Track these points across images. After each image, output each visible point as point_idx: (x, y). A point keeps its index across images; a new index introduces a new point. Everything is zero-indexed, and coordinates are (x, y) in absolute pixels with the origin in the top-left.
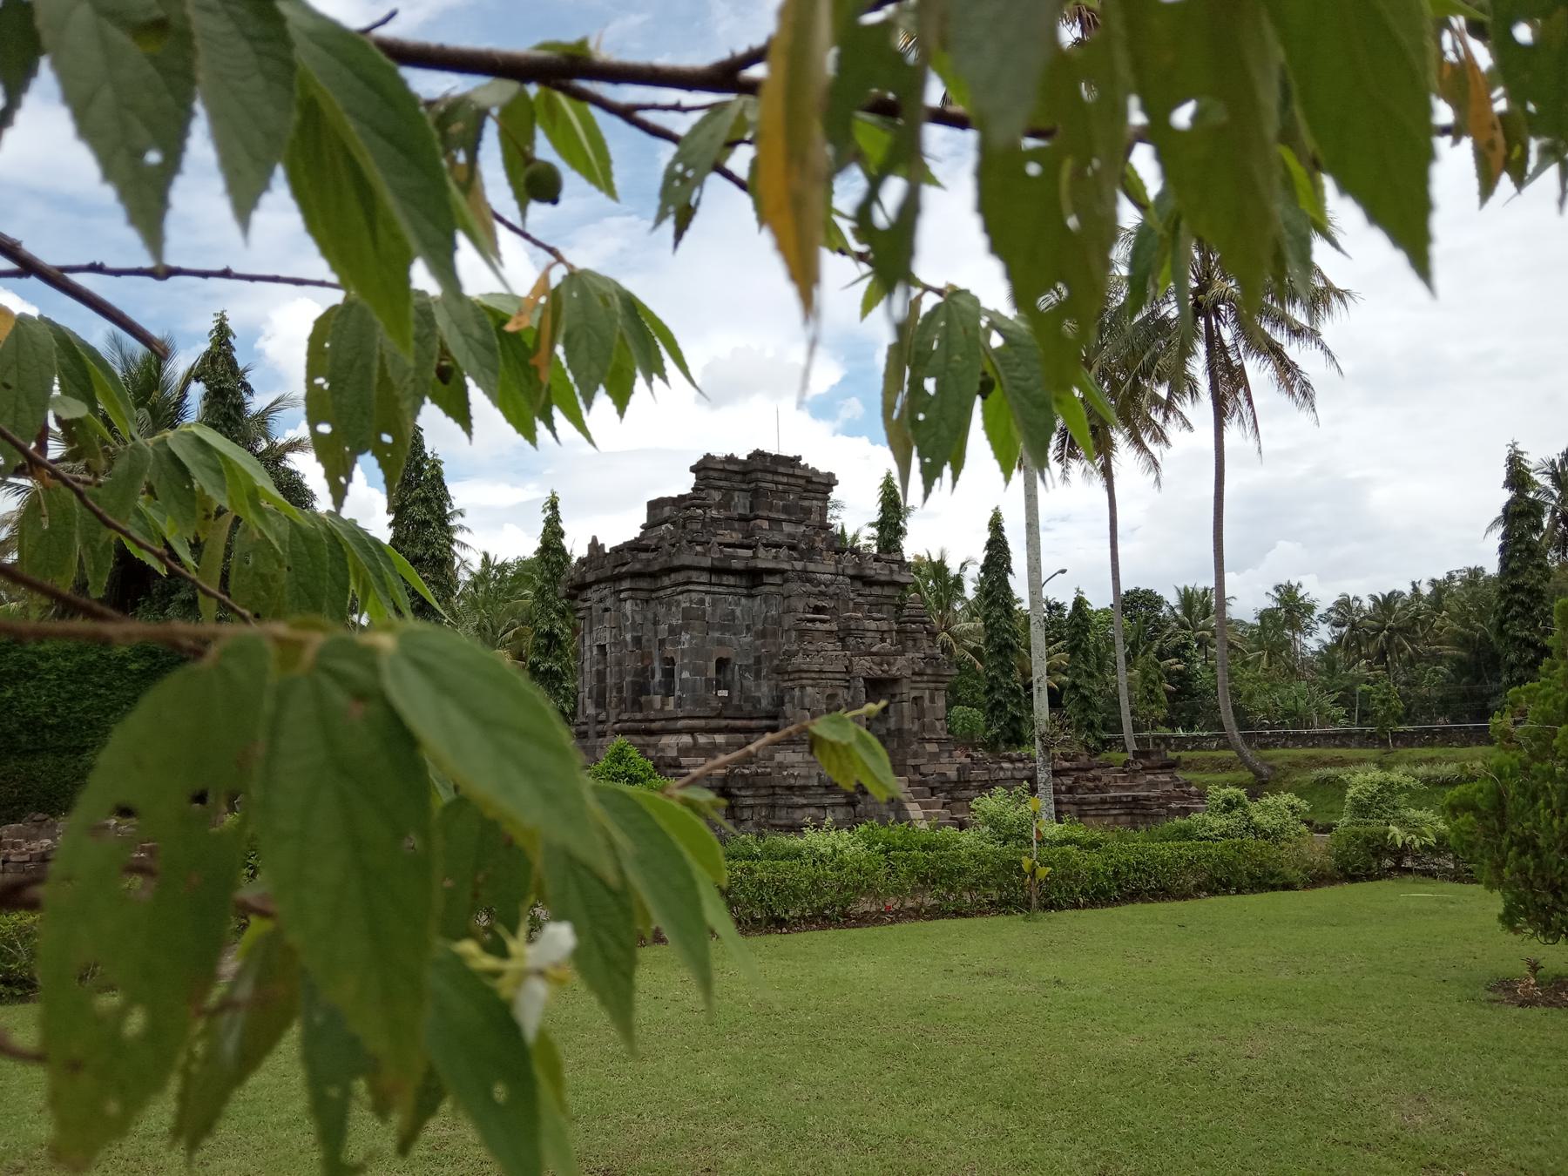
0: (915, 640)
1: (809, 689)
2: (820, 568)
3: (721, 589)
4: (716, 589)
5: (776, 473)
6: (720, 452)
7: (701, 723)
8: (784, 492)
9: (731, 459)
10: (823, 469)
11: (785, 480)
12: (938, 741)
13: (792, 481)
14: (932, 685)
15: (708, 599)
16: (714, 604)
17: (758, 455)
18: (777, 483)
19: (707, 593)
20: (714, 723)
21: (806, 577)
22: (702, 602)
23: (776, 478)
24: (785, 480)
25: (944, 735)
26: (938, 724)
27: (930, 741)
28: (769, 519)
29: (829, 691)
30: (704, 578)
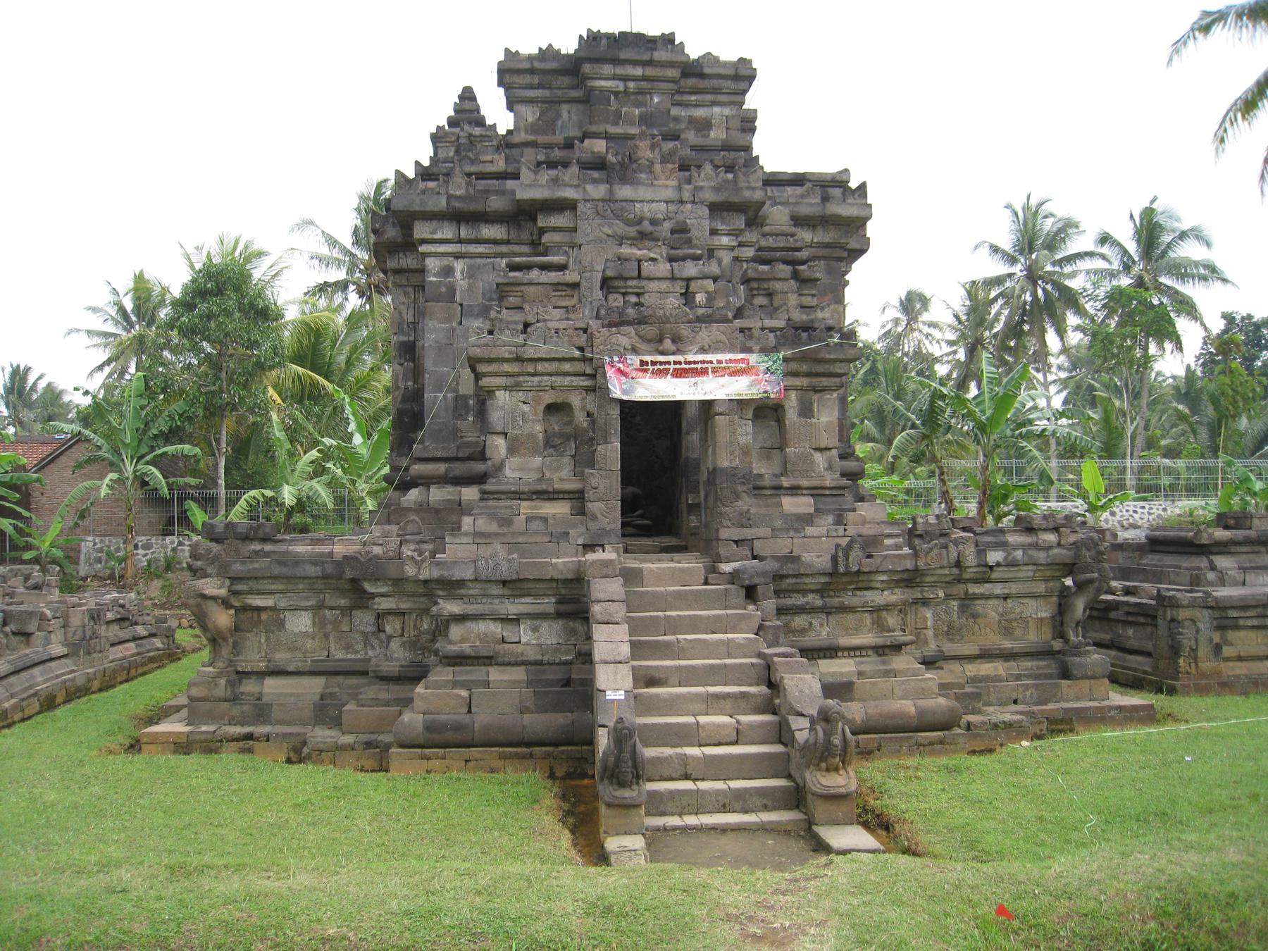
0: (770, 295)
1: (501, 396)
2: (643, 193)
3: (481, 249)
4: (473, 249)
5: (616, 62)
6: (529, 48)
7: (441, 468)
8: (641, 92)
9: (548, 54)
10: (728, 54)
11: (639, 71)
12: (816, 492)
13: (650, 72)
14: (804, 382)
15: (459, 266)
16: (471, 274)
17: (593, 40)
18: (625, 79)
19: (457, 256)
20: (460, 469)
21: (611, 207)
22: (448, 271)
23: (620, 71)
24: (639, 71)
25: (830, 480)
26: (819, 458)
27: (794, 490)
28: (608, 137)
29: (549, 398)
30: (447, 232)
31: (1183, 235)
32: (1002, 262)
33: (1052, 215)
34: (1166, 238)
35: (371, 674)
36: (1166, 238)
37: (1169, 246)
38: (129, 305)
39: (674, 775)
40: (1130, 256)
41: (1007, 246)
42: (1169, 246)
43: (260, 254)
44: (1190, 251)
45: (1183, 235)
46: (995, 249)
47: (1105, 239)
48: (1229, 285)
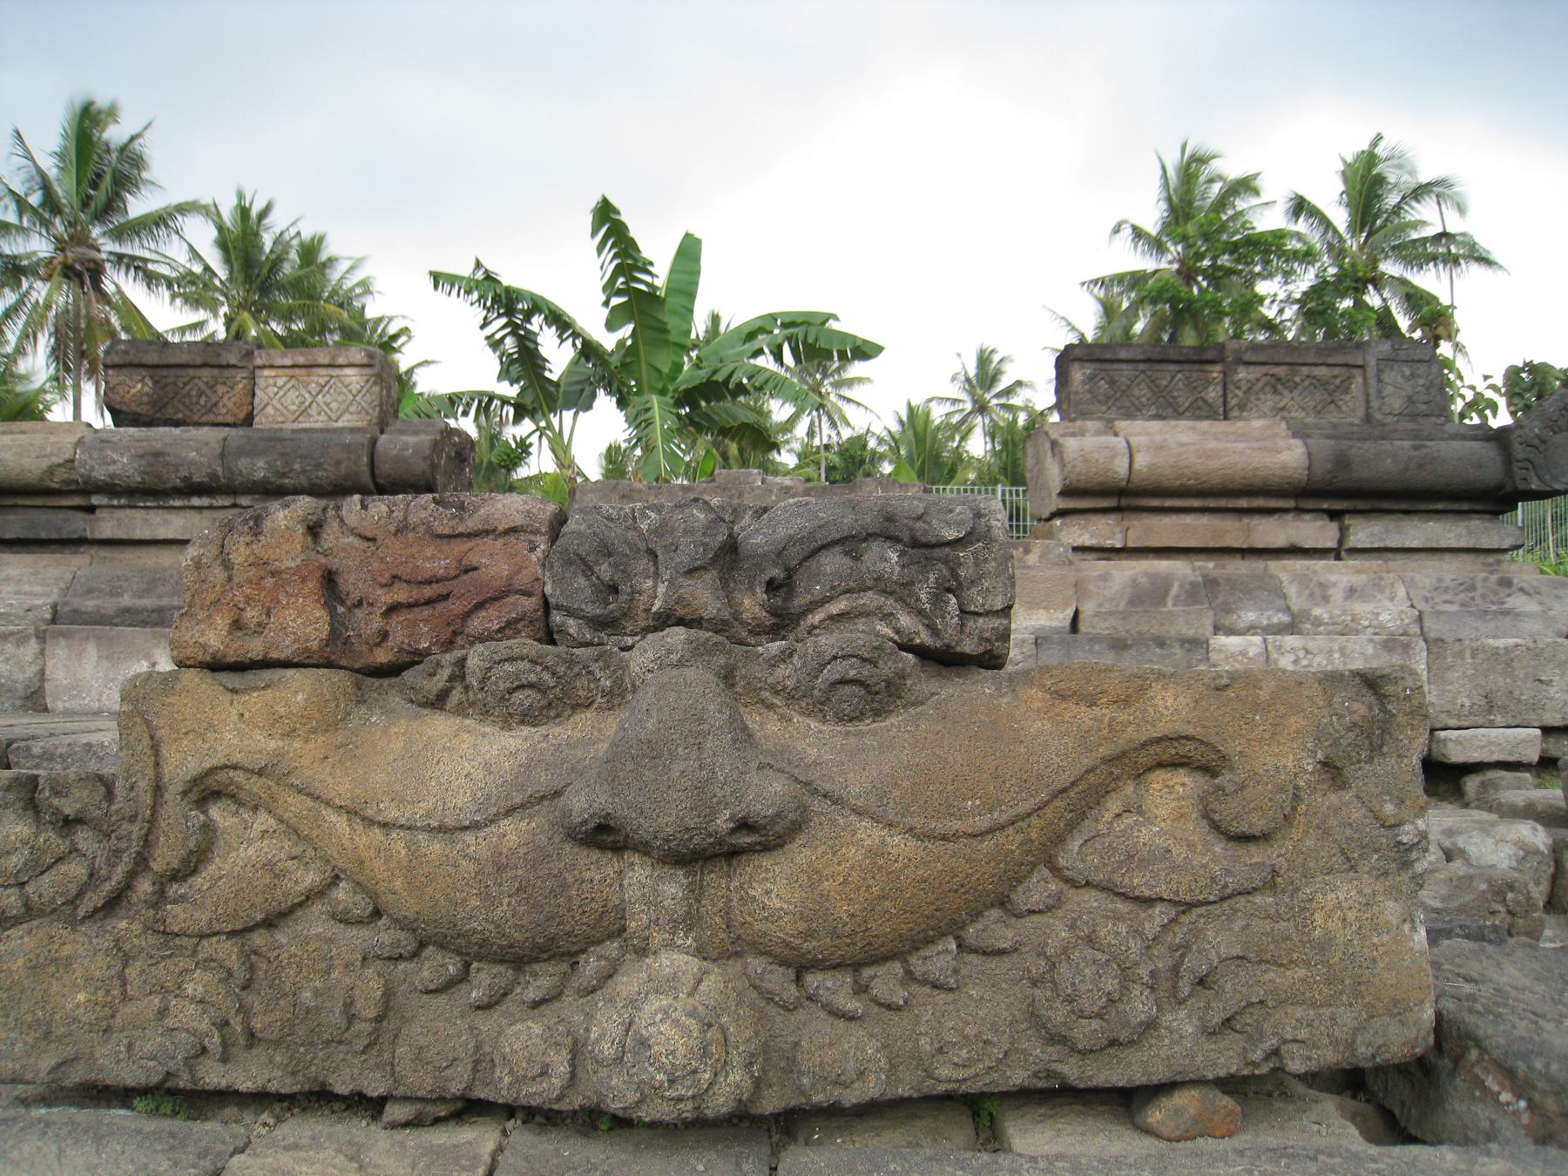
31: (1419, 192)
32: (187, 307)
33: (1221, 178)
34: (1392, 199)
35: (705, 624)
36: (1392, 199)
37: (1397, 209)
38: (905, 418)
39: (1165, 1131)
40: (1335, 231)
41: (1152, 225)
42: (1397, 209)
43: (1256, 192)
44: (1428, 217)
45: (1419, 192)
46: (1138, 233)
47: (1300, 207)
48: (1500, 273)
